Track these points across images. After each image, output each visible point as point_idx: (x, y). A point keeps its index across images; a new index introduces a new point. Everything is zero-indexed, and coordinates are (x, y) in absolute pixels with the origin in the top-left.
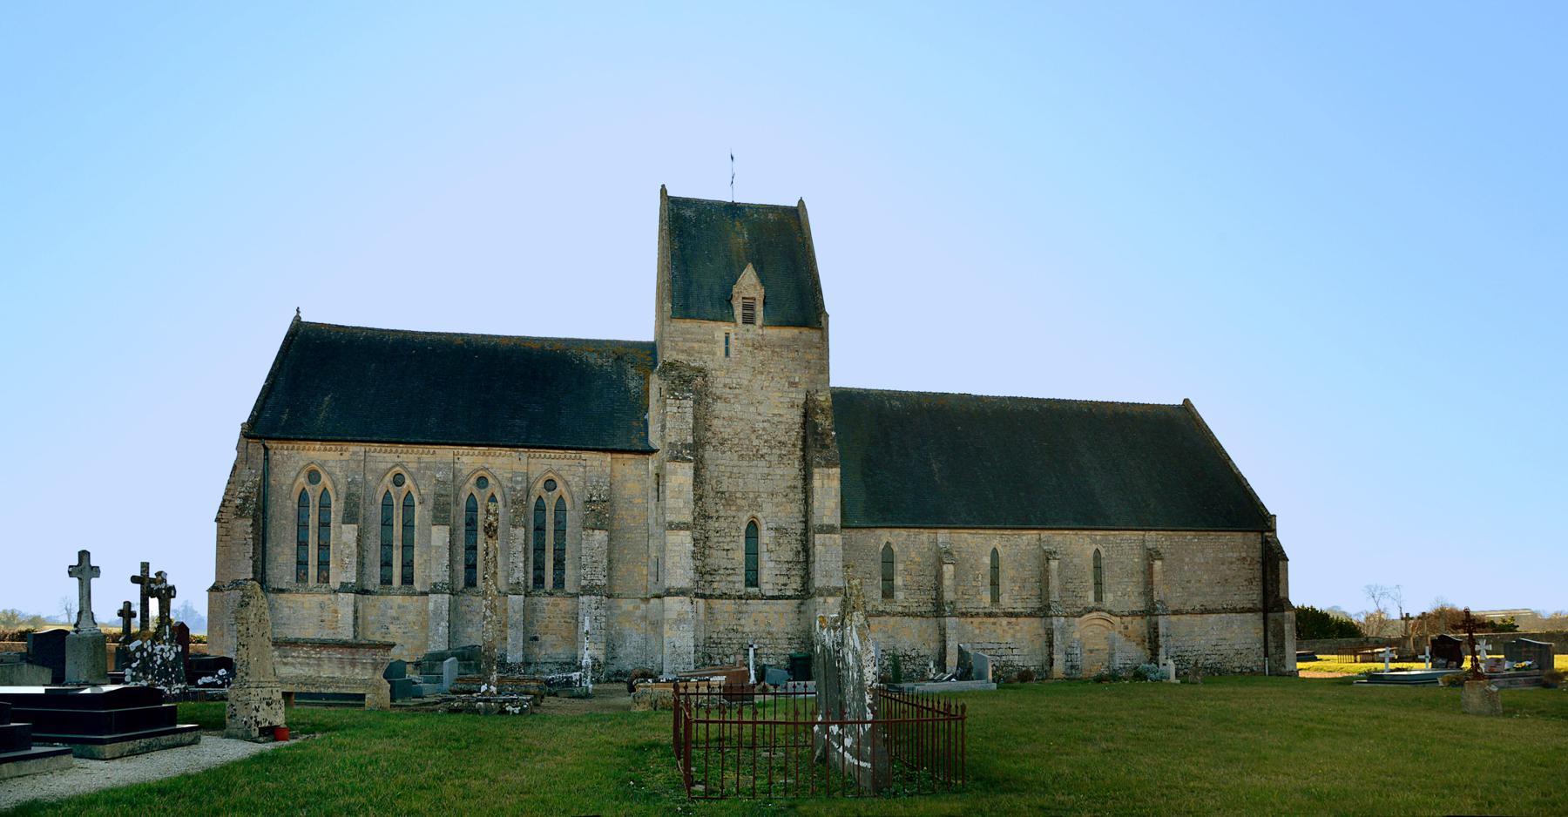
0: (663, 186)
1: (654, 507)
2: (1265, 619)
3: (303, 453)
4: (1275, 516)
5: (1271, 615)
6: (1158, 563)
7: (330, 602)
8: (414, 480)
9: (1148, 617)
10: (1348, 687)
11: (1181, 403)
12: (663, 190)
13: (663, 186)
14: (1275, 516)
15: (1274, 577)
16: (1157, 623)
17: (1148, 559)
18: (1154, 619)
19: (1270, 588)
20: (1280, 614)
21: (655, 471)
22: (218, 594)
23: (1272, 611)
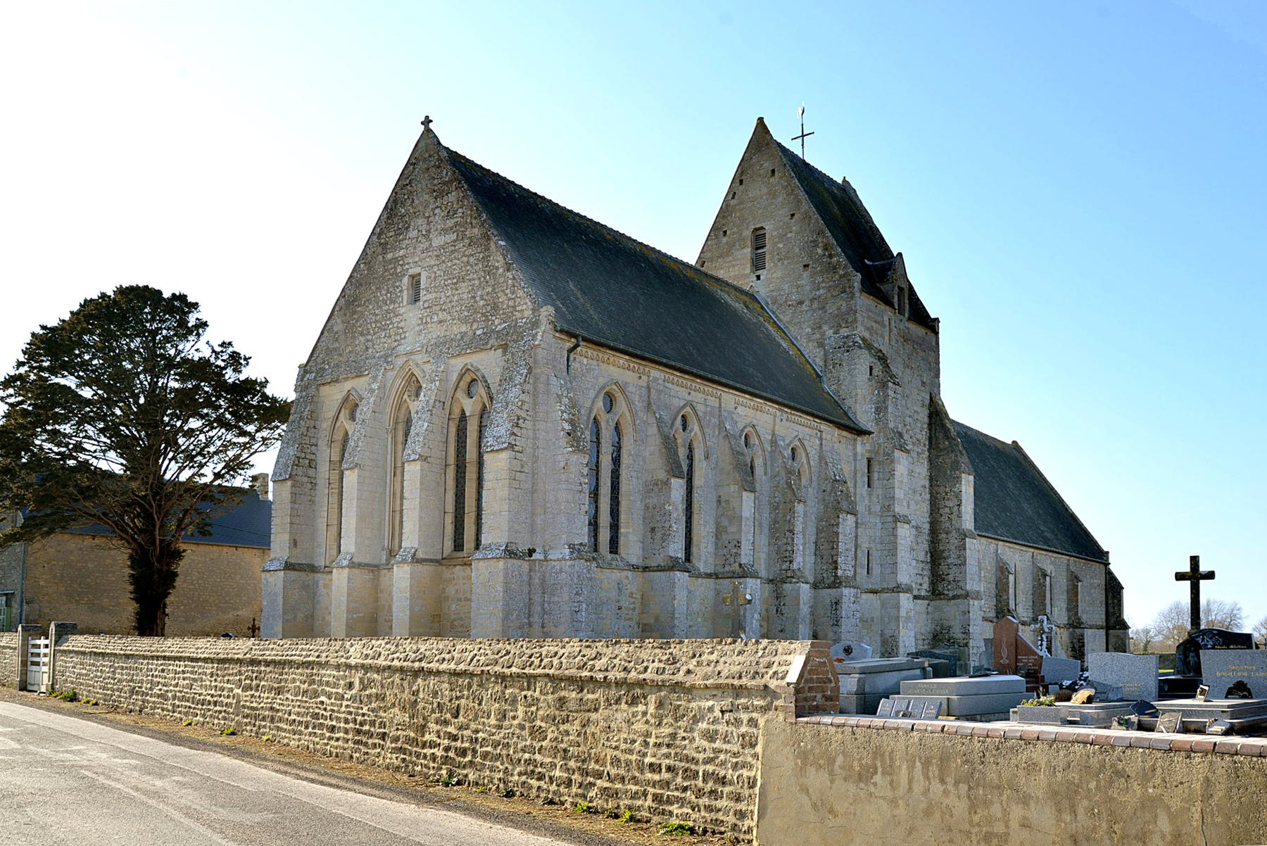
0: (761, 120)
1: (865, 493)
2: (1107, 635)
3: (604, 366)
4: (1108, 553)
5: (1111, 631)
6: (848, 522)
7: (627, 581)
8: (701, 427)
9: (1071, 630)
10: (351, 443)
11: (1010, 442)
12: (427, 121)
13: (761, 120)
14: (1108, 553)
15: (1116, 601)
16: (1082, 635)
17: (1072, 581)
18: (1078, 631)
19: (1111, 610)
20: (1121, 631)
21: (868, 455)
22: (515, 561)
23: (1114, 628)
